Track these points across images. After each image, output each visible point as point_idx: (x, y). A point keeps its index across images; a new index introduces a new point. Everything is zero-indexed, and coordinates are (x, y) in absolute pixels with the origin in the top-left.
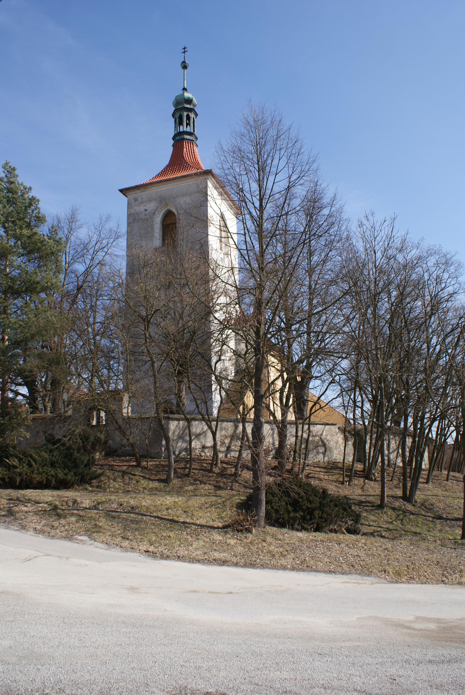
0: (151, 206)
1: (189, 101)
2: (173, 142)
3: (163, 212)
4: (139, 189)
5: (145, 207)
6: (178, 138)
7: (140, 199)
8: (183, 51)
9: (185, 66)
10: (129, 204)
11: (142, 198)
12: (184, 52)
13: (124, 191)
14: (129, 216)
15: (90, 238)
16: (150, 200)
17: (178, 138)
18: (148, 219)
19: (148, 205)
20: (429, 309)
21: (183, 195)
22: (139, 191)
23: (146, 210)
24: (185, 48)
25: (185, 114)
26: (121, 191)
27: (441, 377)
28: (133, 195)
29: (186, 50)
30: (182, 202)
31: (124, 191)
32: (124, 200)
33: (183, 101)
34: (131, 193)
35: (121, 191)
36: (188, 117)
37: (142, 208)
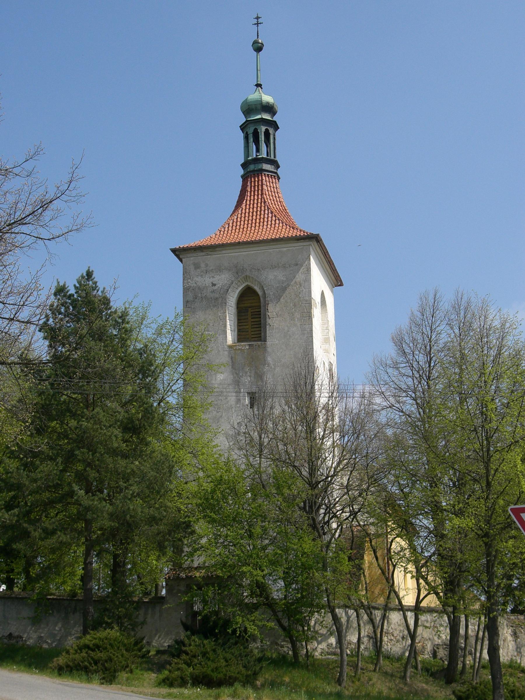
0: (222, 279)
1: (270, 109)
2: (242, 172)
3: (240, 289)
4: (202, 251)
5: (212, 280)
6: (252, 167)
7: (203, 265)
8: (255, 21)
9: (258, 48)
10: (185, 272)
11: (207, 265)
12: (257, 24)
13: (178, 252)
14: (186, 290)
15: (128, 323)
16: (219, 269)
17: (252, 167)
18: (217, 299)
19: (217, 277)
20: (411, 345)
21: (273, 267)
22: (202, 254)
23: (214, 285)
24: (258, 18)
25: (263, 128)
26: (174, 251)
27: (313, 599)
28: (190, 259)
29: (260, 21)
30: (271, 276)
31: (178, 252)
32: (177, 266)
33: (259, 107)
34: (189, 255)
35: (174, 251)
36: (267, 134)
37: (207, 280)
